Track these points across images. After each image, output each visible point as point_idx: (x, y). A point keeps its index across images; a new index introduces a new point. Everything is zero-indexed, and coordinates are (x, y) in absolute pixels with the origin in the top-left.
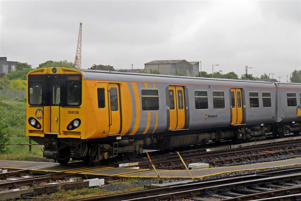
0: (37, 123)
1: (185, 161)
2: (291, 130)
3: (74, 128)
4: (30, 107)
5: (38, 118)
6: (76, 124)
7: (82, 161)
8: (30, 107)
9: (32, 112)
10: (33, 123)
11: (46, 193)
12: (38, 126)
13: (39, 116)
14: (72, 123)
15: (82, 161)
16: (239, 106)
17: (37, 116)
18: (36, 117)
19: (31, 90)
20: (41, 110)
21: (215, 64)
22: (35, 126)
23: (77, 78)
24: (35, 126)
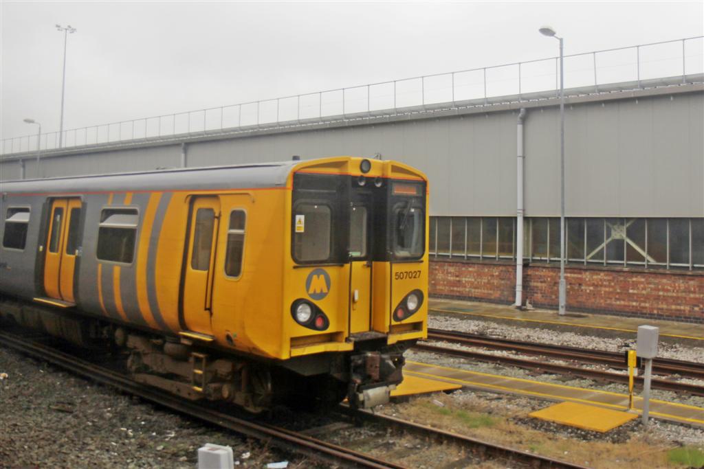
0: (316, 312)
1: (636, 384)
2: (493, 283)
3: (409, 313)
4: (295, 267)
5: (315, 296)
6: (412, 305)
7: (35, 299)
8: (295, 267)
9: (297, 283)
10: (304, 315)
11: (253, 452)
12: (319, 323)
13: (318, 291)
14: (403, 304)
15: (35, 299)
16: (71, 250)
17: (311, 291)
18: (310, 295)
19: (300, 221)
20: (324, 274)
21: (222, 210)
22: (310, 324)
23: (412, 192)
24: (310, 324)
